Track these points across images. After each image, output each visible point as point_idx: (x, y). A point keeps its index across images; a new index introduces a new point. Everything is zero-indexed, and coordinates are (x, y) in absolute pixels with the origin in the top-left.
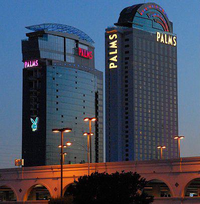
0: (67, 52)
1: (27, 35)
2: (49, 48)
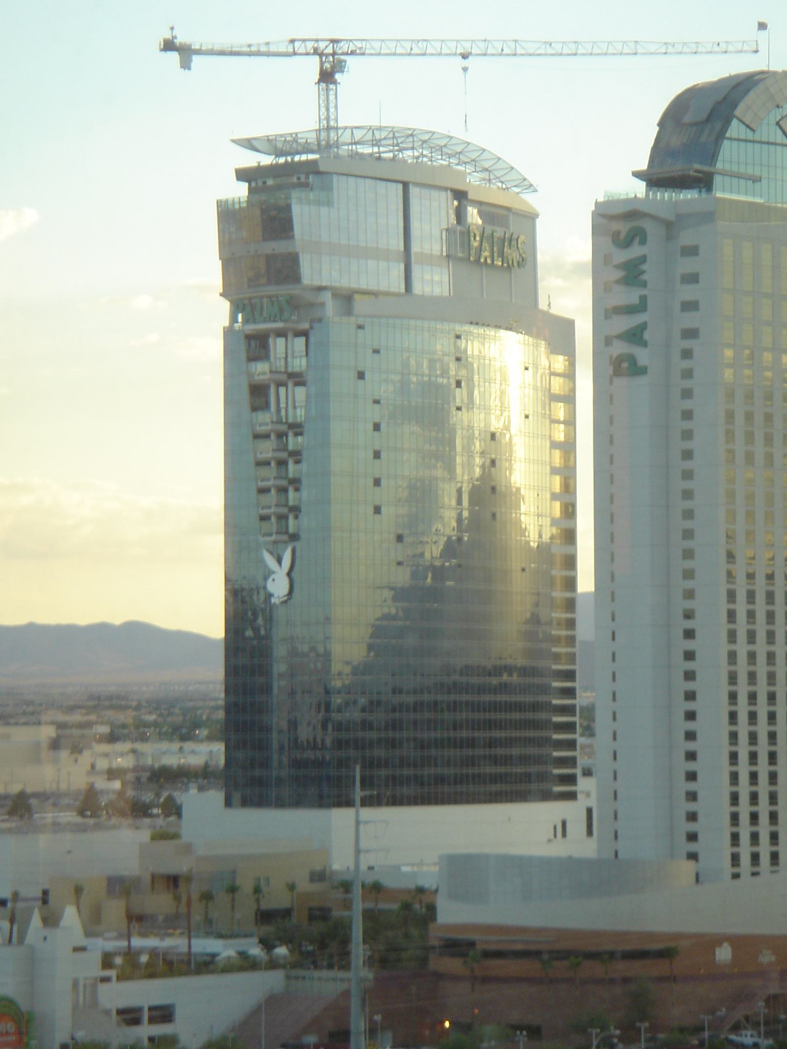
0: (415, 248)
1: (243, 175)
2: (341, 245)
